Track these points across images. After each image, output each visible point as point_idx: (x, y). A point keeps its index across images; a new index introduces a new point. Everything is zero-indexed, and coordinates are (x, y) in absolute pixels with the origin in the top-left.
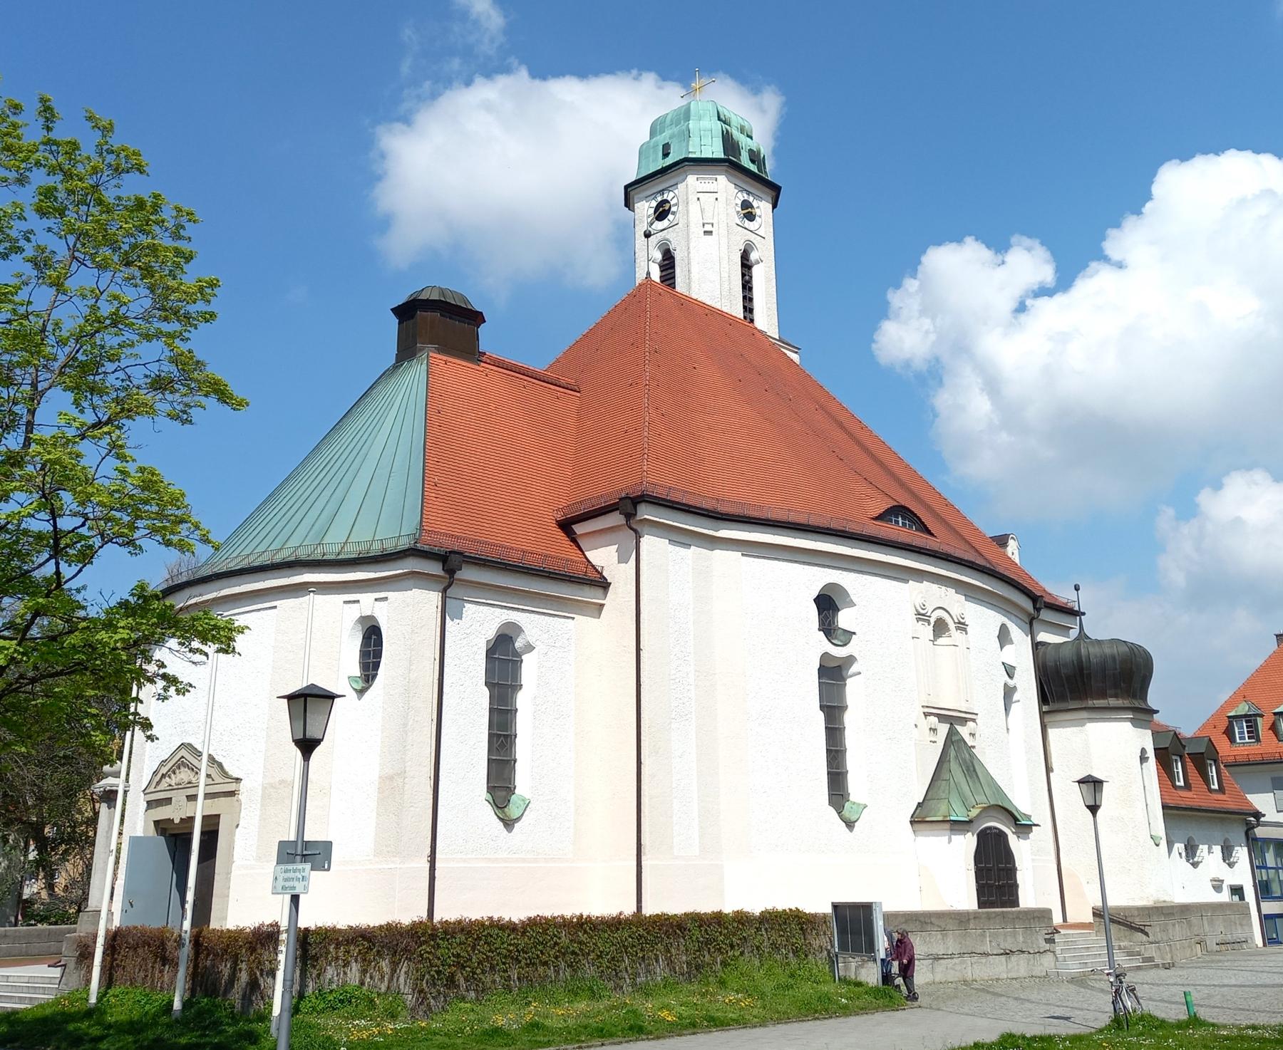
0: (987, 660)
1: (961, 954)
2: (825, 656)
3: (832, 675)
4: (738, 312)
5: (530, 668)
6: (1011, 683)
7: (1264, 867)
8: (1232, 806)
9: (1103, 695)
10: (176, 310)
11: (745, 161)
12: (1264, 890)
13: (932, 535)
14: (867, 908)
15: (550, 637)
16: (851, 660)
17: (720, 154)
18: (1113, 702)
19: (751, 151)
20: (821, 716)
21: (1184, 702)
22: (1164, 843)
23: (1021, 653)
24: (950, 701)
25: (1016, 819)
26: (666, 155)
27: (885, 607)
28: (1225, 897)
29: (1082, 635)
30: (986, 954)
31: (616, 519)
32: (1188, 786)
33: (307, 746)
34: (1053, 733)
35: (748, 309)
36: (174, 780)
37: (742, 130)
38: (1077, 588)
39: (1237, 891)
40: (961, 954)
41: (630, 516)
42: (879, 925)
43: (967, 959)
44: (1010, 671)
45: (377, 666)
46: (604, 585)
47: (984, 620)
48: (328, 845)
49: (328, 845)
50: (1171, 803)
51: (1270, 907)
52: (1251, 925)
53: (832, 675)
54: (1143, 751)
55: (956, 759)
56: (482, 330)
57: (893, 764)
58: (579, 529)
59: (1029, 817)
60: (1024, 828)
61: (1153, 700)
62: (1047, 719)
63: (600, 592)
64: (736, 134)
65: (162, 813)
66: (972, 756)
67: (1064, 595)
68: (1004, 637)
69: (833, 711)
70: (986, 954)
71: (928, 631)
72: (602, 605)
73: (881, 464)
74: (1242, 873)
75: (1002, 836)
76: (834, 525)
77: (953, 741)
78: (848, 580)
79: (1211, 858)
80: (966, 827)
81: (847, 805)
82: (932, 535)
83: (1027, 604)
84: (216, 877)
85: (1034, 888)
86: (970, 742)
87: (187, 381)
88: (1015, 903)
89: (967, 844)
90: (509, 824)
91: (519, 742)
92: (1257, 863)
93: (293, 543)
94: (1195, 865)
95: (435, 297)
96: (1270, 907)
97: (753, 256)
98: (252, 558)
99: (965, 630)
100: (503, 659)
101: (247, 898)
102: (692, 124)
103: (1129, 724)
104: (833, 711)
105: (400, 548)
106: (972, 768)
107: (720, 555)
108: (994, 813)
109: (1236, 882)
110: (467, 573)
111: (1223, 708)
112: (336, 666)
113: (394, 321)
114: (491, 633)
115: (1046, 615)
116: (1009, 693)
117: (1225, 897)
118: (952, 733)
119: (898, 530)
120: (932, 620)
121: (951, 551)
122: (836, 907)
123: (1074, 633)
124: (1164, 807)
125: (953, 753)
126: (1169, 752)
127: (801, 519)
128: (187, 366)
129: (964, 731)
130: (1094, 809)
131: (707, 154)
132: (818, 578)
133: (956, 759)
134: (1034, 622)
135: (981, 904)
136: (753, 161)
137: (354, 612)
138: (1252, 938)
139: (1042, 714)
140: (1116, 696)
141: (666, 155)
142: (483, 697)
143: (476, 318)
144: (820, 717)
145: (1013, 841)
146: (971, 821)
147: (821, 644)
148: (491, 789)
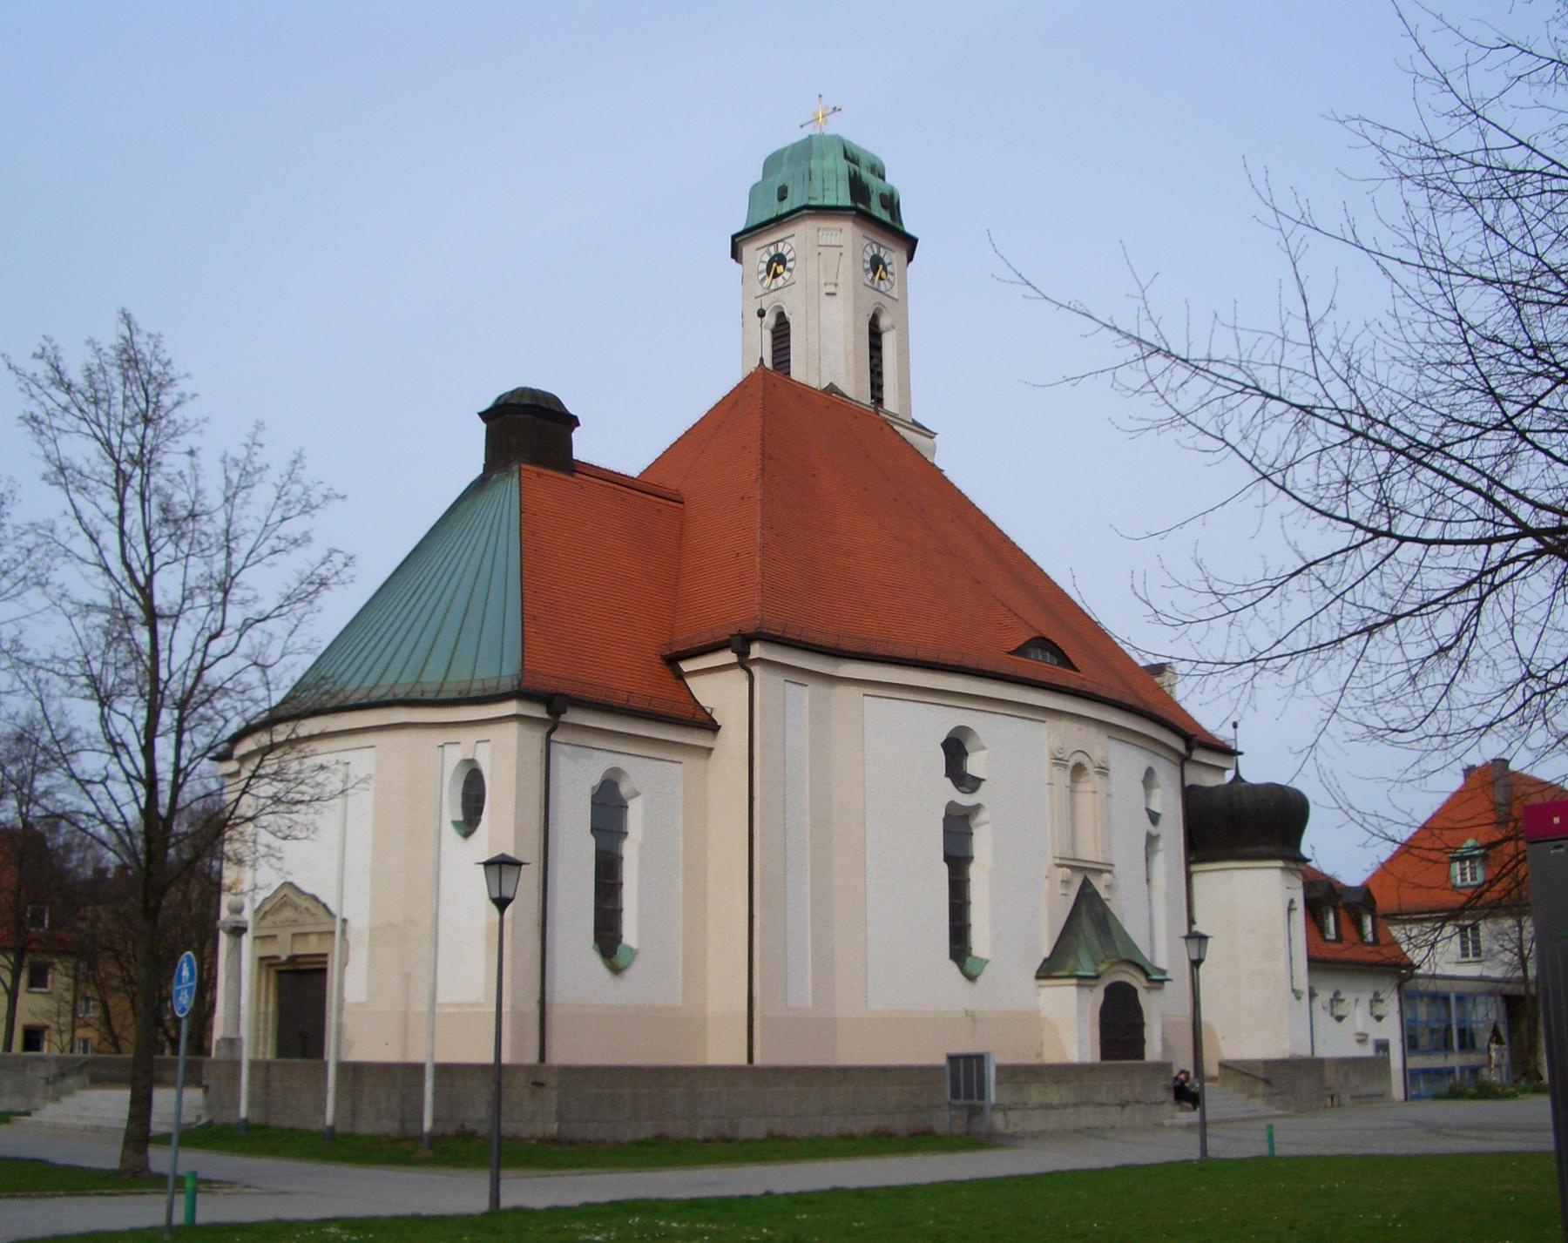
0: (1131, 801)
1: (1076, 1105)
2: (951, 805)
3: (958, 827)
4: (866, 399)
6: (1154, 831)
12: (1411, 1044)
13: (1076, 669)
14: (980, 1058)
15: (655, 784)
17: (845, 200)
18: (1263, 849)
20: (945, 868)
21: (1342, 850)
22: (1305, 998)
23: (1168, 802)
24: (1089, 852)
26: (782, 198)
27: (1020, 748)
29: (1237, 777)
30: (1102, 1105)
31: (728, 657)
33: (502, 903)
34: (1198, 881)
35: (877, 387)
36: (279, 917)
38: (1235, 725)
39: (1382, 1046)
41: (743, 653)
42: (991, 1074)
44: (1154, 818)
45: (480, 810)
46: (712, 727)
47: (1128, 763)
50: (1317, 955)
51: (1417, 1062)
54: (1292, 902)
56: (577, 435)
57: (1018, 910)
58: (686, 666)
59: (1163, 972)
60: (1156, 980)
61: (1305, 850)
62: (1194, 868)
63: (708, 735)
64: (866, 176)
65: (269, 950)
66: (1106, 909)
67: (1223, 733)
68: (1149, 777)
69: (958, 862)
70: (1102, 1105)
71: (1064, 777)
72: (710, 750)
74: (1390, 1030)
75: (1133, 991)
78: (978, 722)
79: (1358, 1016)
80: (1093, 982)
81: (969, 960)
82: (1076, 669)
83: (1179, 745)
86: (1104, 895)
88: (1141, 1056)
89: (1097, 997)
90: (971, 978)
92: (1408, 1015)
93: (389, 680)
94: (1340, 1019)
95: (526, 401)
96: (1417, 1062)
97: (884, 322)
99: (1106, 775)
100: (608, 810)
102: (814, 164)
103: (1277, 873)
104: (958, 862)
107: (842, 691)
108: (1125, 968)
109: (1382, 1036)
110: (573, 716)
113: (478, 431)
114: (596, 780)
115: (1198, 755)
116: (1151, 840)
117: (1368, 1051)
118: (1086, 884)
120: (1071, 764)
122: (952, 1059)
123: (1229, 776)
125: (1084, 907)
126: (1322, 898)
129: (1099, 884)
130: (1196, 964)
131: (830, 201)
132: (945, 720)
135: (1104, 1057)
136: (884, 207)
137: (454, 756)
138: (1390, 1091)
139: (1188, 863)
141: (782, 198)
142: (589, 845)
143: (573, 422)
144: (943, 870)
145: (1144, 998)
146: (1097, 977)
147: (948, 792)
148: (598, 938)
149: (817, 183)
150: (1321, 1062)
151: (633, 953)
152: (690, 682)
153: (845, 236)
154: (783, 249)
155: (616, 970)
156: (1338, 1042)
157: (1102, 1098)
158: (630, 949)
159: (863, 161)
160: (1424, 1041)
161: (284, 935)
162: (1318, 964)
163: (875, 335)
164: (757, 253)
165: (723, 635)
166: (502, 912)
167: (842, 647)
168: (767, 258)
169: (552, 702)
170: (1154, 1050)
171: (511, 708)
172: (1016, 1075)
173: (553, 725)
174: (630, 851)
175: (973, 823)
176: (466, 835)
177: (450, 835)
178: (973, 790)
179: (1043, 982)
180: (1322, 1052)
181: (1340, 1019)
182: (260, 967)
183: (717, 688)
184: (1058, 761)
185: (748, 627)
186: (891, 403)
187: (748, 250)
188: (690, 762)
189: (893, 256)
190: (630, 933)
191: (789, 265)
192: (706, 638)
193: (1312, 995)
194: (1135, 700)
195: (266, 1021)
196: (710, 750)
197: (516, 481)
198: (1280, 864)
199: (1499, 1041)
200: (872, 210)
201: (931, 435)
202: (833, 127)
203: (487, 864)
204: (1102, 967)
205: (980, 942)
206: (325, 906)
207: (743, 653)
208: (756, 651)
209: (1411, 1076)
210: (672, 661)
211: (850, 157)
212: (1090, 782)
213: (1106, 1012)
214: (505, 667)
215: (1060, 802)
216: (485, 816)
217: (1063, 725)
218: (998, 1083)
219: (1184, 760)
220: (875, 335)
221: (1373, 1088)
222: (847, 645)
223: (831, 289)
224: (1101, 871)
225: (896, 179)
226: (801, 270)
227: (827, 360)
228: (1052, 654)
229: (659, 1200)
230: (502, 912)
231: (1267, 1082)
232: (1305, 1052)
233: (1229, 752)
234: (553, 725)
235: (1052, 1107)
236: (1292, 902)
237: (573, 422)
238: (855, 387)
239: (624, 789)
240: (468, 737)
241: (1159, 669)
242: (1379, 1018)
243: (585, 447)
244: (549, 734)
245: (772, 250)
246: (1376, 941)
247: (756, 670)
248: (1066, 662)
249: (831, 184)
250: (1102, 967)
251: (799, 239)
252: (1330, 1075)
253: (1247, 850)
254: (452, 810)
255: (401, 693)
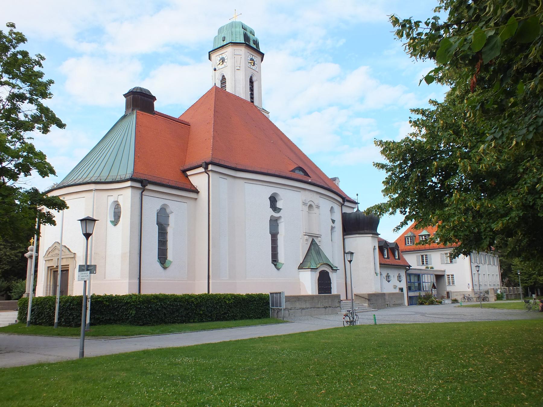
1: (311, 308)
3: (274, 223)
5: (172, 220)
6: (333, 225)
7: (410, 282)
8: (402, 264)
9: (364, 230)
10: (41, 89)
11: (252, 44)
12: (409, 289)
15: (178, 209)
16: (280, 217)
18: (366, 231)
19: (254, 41)
22: (379, 275)
24: (315, 232)
25: (332, 268)
27: (292, 199)
28: (397, 291)
31: (202, 170)
32: (388, 258)
33: (87, 235)
35: (252, 98)
37: (251, 32)
38: (357, 195)
39: (401, 290)
40: (311, 308)
41: (206, 168)
43: (312, 309)
44: (333, 221)
46: (197, 192)
48: (95, 266)
49: (95, 266)
50: (383, 263)
52: (404, 299)
53: (274, 223)
54: (375, 246)
55: (314, 249)
56: (155, 103)
57: (292, 249)
58: (189, 173)
59: (337, 267)
60: (334, 270)
61: (379, 231)
62: (345, 237)
64: (249, 34)
66: (319, 248)
67: (353, 197)
71: (306, 208)
73: (295, 153)
74: (403, 285)
75: (327, 273)
76: (277, 173)
77: (313, 243)
84: (69, 284)
85: (336, 288)
87: (47, 120)
89: (316, 275)
90: (278, 269)
91: (168, 243)
94: (389, 281)
96: (411, 294)
97: (254, 79)
98: (76, 181)
101: (76, 289)
105: (126, 178)
106: (319, 252)
108: (325, 266)
109: (401, 287)
110: (149, 187)
111: (403, 234)
112: (104, 217)
114: (159, 208)
115: (346, 204)
116: (332, 228)
117: (397, 291)
118: (313, 240)
119: (299, 175)
120: (308, 205)
121: (315, 182)
123: (355, 210)
124: (380, 264)
125: (313, 247)
127: (265, 171)
128: (44, 110)
129: (317, 240)
132: (269, 191)
133: (314, 249)
134: (343, 207)
136: (254, 44)
137: (111, 200)
139: (344, 235)
140: (367, 230)
143: (154, 98)
144: (269, 236)
147: (271, 212)
149: (234, 35)
150: (384, 294)
151: (171, 262)
152: (190, 178)
153: (242, 51)
154: (224, 56)
155: (165, 268)
156: (389, 288)
157: (319, 306)
158: (170, 261)
159: (248, 30)
160: (413, 288)
161: (55, 259)
162: (383, 265)
163: (251, 82)
164: (216, 57)
165: (199, 163)
166: (87, 239)
167: (238, 167)
168: (219, 59)
169: (142, 183)
170: (335, 291)
171: (129, 184)
172: (289, 299)
173: (143, 189)
174: (170, 231)
175: (278, 222)
176: (115, 225)
177: (110, 225)
178: (279, 212)
179: (300, 270)
180: (385, 291)
181: (389, 281)
182: (48, 269)
183: (199, 179)
184: (304, 204)
185: (208, 160)
186: (256, 103)
187: (213, 56)
188: (191, 202)
189: (257, 59)
190: (170, 256)
191: (226, 61)
192: (196, 164)
193: (381, 274)
194: (329, 188)
195: (50, 288)
196: (196, 199)
197: (135, 116)
198: (371, 235)
199: (435, 288)
200: (250, 44)
201: (268, 113)
202: (238, 20)
203: (81, 220)
204: (318, 266)
205: (281, 258)
206: (68, 249)
207: (206, 168)
208: (210, 167)
209: (410, 298)
210: (184, 172)
211: (244, 28)
212: (316, 210)
213: (319, 279)
214: (128, 170)
215: (305, 216)
216: (121, 219)
217: (307, 193)
218: (286, 301)
219: (342, 205)
220: (251, 82)
221: (399, 302)
222: (238, 167)
223: (238, 68)
224: (318, 237)
225: (258, 36)
226: (229, 62)
227: (237, 87)
228: (303, 173)
229: (120, 354)
230: (87, 239)
231: (369, 300)
232: (379, 291)
233: (356, 203)
234: (143, 189)
235: (303, 309)
236: (375, 246)
237: (154, 98)
238: (244, 95)
239: (168, 211)
240: (115, 194)
241: (334, 179)
242: (400, 281)
243: (158, 106)
244: (142, 193)
245: (221, 56)
246: (399, 259)
247: (210, 173)
248: (306, 174)
249: (238, 36)
250: (318, 266)
251: (228, 52)
252: (387, 297)
253: (361, 232)
254: (110, 217)
255: (93, 180)
